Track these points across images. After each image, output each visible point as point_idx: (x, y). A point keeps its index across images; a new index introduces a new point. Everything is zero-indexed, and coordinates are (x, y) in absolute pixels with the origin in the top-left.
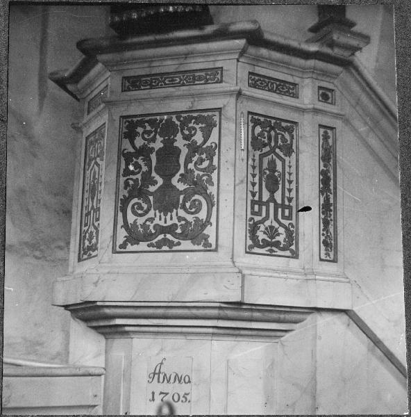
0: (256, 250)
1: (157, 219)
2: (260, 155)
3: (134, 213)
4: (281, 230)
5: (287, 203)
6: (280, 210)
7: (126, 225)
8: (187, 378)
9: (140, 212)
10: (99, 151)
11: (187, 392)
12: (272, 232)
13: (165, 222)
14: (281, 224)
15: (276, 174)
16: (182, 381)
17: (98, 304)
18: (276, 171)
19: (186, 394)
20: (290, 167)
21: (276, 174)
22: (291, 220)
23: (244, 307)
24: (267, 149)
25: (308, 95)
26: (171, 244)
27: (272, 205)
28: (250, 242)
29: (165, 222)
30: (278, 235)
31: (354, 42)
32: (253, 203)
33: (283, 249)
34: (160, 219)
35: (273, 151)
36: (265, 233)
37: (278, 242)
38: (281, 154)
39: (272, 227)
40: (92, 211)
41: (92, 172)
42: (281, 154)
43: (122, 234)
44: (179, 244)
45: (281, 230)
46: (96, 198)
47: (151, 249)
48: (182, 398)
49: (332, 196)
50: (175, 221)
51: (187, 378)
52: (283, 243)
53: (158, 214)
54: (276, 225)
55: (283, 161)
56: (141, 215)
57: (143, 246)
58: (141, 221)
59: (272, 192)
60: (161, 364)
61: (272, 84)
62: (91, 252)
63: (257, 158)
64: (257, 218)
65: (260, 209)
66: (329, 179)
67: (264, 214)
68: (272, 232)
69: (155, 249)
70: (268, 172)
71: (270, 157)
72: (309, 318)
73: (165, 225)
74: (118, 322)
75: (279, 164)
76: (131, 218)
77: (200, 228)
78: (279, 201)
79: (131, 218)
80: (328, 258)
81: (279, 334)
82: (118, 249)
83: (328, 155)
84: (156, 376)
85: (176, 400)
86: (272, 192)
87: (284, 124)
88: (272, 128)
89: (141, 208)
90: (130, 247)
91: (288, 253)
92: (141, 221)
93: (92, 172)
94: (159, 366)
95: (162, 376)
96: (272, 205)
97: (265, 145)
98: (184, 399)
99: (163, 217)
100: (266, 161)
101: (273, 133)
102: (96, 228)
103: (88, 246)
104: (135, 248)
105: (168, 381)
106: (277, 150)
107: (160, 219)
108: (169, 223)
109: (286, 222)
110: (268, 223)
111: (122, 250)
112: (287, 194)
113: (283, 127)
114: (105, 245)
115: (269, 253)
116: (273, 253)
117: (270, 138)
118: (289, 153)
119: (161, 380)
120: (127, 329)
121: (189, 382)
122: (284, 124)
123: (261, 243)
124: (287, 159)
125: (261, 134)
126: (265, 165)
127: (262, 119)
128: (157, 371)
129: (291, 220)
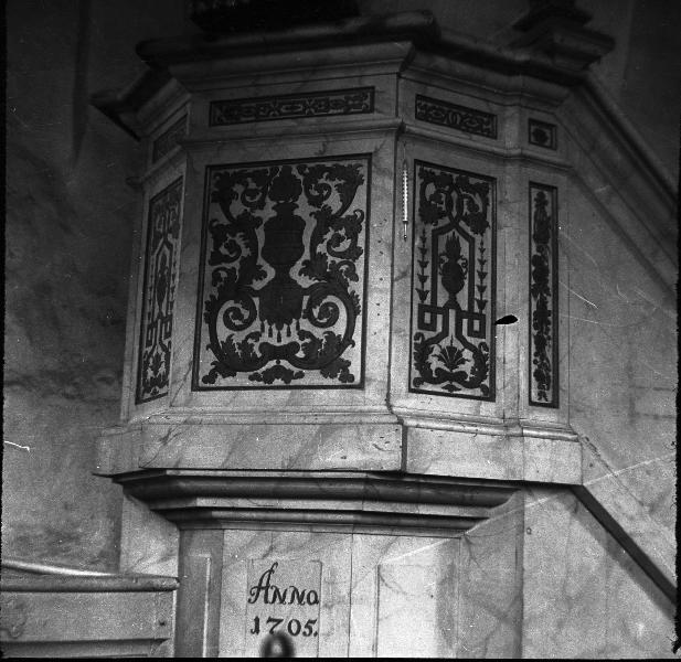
1: (266, 334)
4: (467, 354)
5: (477, 310)
6: (465, 321)
9: (237, 322)
12: (452, 357)
15: (460, 262)
16: (305, 600)
18: (461, 257)
19: (310, 622)
20: (482, 251)
21: (460, 262)
23: (487, 485)
24: (445, 221)
25: (511, 135)
27: (452, 313)
28: (416, 374)
30: (463, 362)
32: (423, 309)
33: (470, 386)
34: (271, 335)
35: (454, 224)
36: (440, 358)
37: (463, 374)
38: (468, 230)
39: (451, 349)
41: (160, 257)
42: (468, 230)
43: (208, 359)
44: (301, 375)
45: (467, 354)
47: (256, 383)
48: (303, 629)
49: (550, 299)
50: (295, 338)
53: (267, 327)
54: (458, 345)
55: (472, 241)
58: (238, 338)
61: (454, 114)
63: (429, 235)
64: (428, 335)
65: (434, 320)
67: (440, 328)
70: (446, 259)
71: (450, 234)
73: (278, 345)
74: (202, 502)
75: (465, 246)
76: (223, 333)
78: (465, 307)
79: (223, 333)
80: (543, 401)
84: (262, 593)
87: (473, 181)
88: (454, 187)
90: (221, 381)
91: (478, 392)
93: (160, 257)
96: (452, 313)
97: (441, 215)
98: (307, 631)
99: (275, 331)
100: (443, 240)
101: (454, 195)
105: (282, 601)
106: (462, 224)
107: (271, 335)
108: (285, 341)
110: (445, 343)
119: (270, 598)
120: (216, 514)
121: (316, 602)
122: (473, 181)
124: (478, 238)
125: (436, 197)
126: (442, 248)
127: (437, 172)
128: (264, 585)
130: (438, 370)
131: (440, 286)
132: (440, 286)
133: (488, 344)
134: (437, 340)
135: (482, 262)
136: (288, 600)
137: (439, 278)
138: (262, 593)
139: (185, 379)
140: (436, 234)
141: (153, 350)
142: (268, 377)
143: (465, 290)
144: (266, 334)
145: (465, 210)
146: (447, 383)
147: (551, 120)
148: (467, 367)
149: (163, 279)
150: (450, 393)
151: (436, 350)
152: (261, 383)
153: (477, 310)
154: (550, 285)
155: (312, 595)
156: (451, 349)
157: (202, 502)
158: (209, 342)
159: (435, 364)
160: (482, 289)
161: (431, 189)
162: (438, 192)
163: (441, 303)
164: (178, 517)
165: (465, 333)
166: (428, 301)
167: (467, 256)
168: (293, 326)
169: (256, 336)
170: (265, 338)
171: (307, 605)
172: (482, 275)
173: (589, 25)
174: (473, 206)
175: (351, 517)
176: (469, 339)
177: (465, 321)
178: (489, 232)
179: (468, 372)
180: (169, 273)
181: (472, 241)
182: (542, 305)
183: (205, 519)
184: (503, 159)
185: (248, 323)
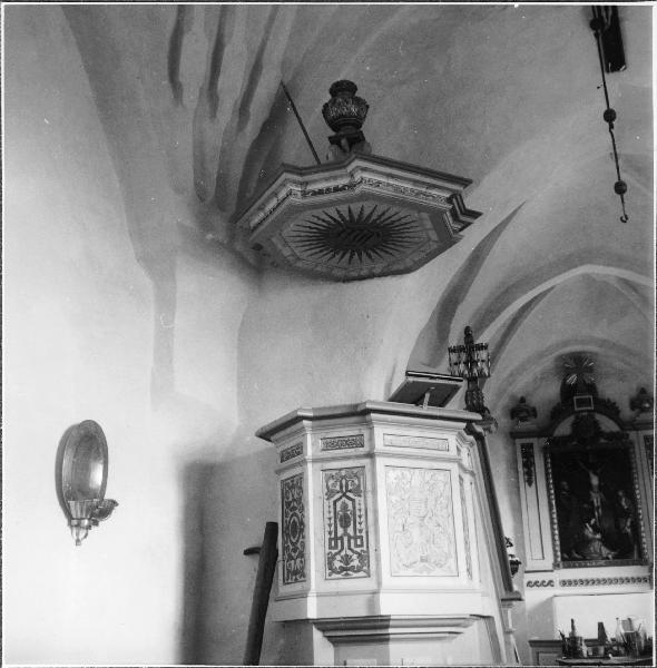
40: (346, 539)
45: (355, 556)
54: (349, 553)
57: (410, 572)
110: (343, 553)
124: (357, 499)
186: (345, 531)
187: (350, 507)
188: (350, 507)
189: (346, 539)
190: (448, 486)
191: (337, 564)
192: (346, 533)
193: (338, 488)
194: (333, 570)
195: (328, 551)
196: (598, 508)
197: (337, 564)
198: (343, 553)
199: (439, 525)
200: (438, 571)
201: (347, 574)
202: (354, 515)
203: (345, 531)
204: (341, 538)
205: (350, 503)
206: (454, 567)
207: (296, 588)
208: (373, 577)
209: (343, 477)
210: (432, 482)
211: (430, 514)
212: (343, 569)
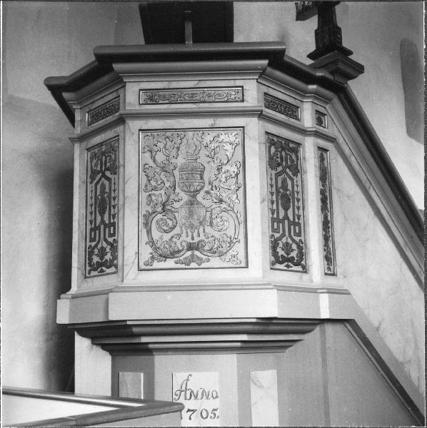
0: (278, 266)
1: (184, 235)
2: (276, 174)
3: (159, 228)
4: (294, 246)
5: (297, 220)
6: (292, 227)
7: (152, 243)
8: (214, 393)
9: (165, 228)
10: (108, 165)
11: (215, 408)
12: (287, 248)
13: (193, 239)
14: (293, 240)
15: (288, 192)
16: (210, 396)
17: (128, 323)
18: (288, 190)
19: (214, 410)
20: (297, 186)
21: (288, 192)
22: (301, 236)
23: (274, 321)
24: (280, 169)
25: (307, 117)
26: (200, 261)
27: (286, 222)
28: (273, 259)
29: (193, 239)
30: (292, 250)
31: (349, 70)
32: (273, 220)
33: (296, 265)
34: (187, 236)
35: (284, 171)
36: (283, 249)
37: (293, 258)
38: (290, 173)
39: (287, 243)
40: (102, 227)
41: (99, 187)
42: (290, 173)
43: (146, 252)
44: (209, 260)
45: (294, 246)
46: (107, 212)
47: (179, 266)
48: (210, 415)
49: (329, 214)
50: (202, 237)
51: (214, 393)
52: (296, 258)
53: (184, 231)
54: (290, 241)
55: (292, 180)
56: (166, 232)
57: (170, 263)
58: (167, 237)
59: (286, 209)
60: (188, 380)
61: (281, 105)
62: (104, 268)
63: (273, 177)
64: (277, 235)
65: (278, 227)
66: (326, 198)
67: (281, 232)
68: (287, 248)
69: (183, 266)
70: (282, 191)
71: (283, 176)
72: (318, 329)
73: (192, 242)
74: (144, 340)
75: (289, 182)
76: (156, 234)
77: (228, 245)
78: (291, 218)
79: (156, 234)
80: (329, 272)
81: (287, 344)
82: (143, 267)
83: (324, 175)
84: (183, 393)
85: (204, 416)
86: (286, 209)
87: (291, 145)
88: (283, 149)
89: (166, 224)
90: (156, 265)
91: (299, 268)
92: (167, 237)
93: (99, 187)
94: (185, 382)
95: (188, 393)
96: (286, 222)
97: (279, 165)
98: (213, 415)
99: (190, 234)
100: (280, 179)
101: (283, 153)
102: (112, 245)
103: (97, 262)
104: (162, 265)
105: (196, 397)
106: (288, 170)
107: (187, 236)
108: (196, 240)
109: (297, 239)
110: (284, 240)
111: (149, 267)
112: (296, 212)
113: (290, 148)
114: (131, 261)
115: (286, 268)
116: (290, 269)
117: (282, 160)
118: (295, 174)
119: (188, 397)
120: (150, 346)
121: (217, 397)
122: (291, 145)
123: (281, 259)
124: (295, 178)
125: (275, 154)
126: (280, 185)
127: (275, 139)
128: (184, 388)
129: (301, 236)
130: (282, 255)
131: (280, 207)
132: (280, 207)
133: (303, 241)
134: (280, 238)
135: (298, 193)
136: (199, 396)
137: (280, 201)
138: (183, 393)
139: (133, 263)
140: (278, 175)
141: (96, 246)
142: (188, 262)
143: (291, 209)
144: (184, 235)
145: (289, 163)
146: (286, 263)
147: (325, 112)
148: (294, 254)
149: (103, 200)
150: (288, 268)
151: (281, 245)
152: (183, 266)
153: (297, 220)
154: (328, 206)
155: (214, 393)
156: (287, 243)
157: (144, 340)
158: (147, 240)
159: (281, 252)
160: (298, 208)
161: (273, 149)
162: (276, 151)
163: (281, 217)
164: (111, 347)
165: (292, 234)
166: (275, 216)
167: (291, 189)
168: (201, 230)
169: (179, 236)
170: (183, 237)
171: (212, 399)
172: (298, 200)
173: (350, 57)
174: (292, 161)
175: (239, 344)
176: (294, 237)
177: (292, 227)
178: (299, 175)
179: (295, 256)
180: (109, 197)
181: (292, 180)
182: (326, 217)
183: (146, 350)
184: (303, 132)
185: (173, 228)
186: (102, 218)
187: (107, 187)
188: (107, 187)
189: (102, 227)
190: (239, 149)
191: (96, 259)
192: (103, 221)
193: (99, 169)
194: (111, 264)
195: (88, 244)
196: (115, 132)
197: (96, 259)
198: (99, 246)
199: (221, 201)
200: (215, 261)
201: (102, 271)
202: (293, 197)
203: (102, 218)
204: (99, 228)
205: (107, 183)
206: (241, 256)
207: (98, 283)
208: (120, 273)
209: (103, 154)
210: (212, 146)
211: (207, 188)
212: (100, 265)
